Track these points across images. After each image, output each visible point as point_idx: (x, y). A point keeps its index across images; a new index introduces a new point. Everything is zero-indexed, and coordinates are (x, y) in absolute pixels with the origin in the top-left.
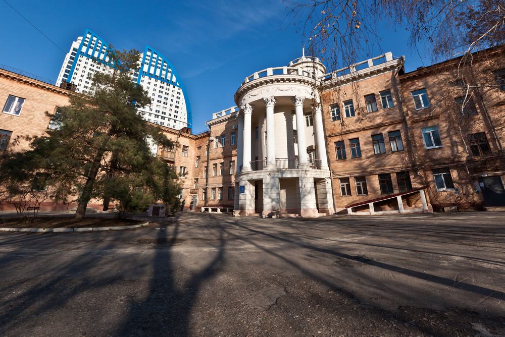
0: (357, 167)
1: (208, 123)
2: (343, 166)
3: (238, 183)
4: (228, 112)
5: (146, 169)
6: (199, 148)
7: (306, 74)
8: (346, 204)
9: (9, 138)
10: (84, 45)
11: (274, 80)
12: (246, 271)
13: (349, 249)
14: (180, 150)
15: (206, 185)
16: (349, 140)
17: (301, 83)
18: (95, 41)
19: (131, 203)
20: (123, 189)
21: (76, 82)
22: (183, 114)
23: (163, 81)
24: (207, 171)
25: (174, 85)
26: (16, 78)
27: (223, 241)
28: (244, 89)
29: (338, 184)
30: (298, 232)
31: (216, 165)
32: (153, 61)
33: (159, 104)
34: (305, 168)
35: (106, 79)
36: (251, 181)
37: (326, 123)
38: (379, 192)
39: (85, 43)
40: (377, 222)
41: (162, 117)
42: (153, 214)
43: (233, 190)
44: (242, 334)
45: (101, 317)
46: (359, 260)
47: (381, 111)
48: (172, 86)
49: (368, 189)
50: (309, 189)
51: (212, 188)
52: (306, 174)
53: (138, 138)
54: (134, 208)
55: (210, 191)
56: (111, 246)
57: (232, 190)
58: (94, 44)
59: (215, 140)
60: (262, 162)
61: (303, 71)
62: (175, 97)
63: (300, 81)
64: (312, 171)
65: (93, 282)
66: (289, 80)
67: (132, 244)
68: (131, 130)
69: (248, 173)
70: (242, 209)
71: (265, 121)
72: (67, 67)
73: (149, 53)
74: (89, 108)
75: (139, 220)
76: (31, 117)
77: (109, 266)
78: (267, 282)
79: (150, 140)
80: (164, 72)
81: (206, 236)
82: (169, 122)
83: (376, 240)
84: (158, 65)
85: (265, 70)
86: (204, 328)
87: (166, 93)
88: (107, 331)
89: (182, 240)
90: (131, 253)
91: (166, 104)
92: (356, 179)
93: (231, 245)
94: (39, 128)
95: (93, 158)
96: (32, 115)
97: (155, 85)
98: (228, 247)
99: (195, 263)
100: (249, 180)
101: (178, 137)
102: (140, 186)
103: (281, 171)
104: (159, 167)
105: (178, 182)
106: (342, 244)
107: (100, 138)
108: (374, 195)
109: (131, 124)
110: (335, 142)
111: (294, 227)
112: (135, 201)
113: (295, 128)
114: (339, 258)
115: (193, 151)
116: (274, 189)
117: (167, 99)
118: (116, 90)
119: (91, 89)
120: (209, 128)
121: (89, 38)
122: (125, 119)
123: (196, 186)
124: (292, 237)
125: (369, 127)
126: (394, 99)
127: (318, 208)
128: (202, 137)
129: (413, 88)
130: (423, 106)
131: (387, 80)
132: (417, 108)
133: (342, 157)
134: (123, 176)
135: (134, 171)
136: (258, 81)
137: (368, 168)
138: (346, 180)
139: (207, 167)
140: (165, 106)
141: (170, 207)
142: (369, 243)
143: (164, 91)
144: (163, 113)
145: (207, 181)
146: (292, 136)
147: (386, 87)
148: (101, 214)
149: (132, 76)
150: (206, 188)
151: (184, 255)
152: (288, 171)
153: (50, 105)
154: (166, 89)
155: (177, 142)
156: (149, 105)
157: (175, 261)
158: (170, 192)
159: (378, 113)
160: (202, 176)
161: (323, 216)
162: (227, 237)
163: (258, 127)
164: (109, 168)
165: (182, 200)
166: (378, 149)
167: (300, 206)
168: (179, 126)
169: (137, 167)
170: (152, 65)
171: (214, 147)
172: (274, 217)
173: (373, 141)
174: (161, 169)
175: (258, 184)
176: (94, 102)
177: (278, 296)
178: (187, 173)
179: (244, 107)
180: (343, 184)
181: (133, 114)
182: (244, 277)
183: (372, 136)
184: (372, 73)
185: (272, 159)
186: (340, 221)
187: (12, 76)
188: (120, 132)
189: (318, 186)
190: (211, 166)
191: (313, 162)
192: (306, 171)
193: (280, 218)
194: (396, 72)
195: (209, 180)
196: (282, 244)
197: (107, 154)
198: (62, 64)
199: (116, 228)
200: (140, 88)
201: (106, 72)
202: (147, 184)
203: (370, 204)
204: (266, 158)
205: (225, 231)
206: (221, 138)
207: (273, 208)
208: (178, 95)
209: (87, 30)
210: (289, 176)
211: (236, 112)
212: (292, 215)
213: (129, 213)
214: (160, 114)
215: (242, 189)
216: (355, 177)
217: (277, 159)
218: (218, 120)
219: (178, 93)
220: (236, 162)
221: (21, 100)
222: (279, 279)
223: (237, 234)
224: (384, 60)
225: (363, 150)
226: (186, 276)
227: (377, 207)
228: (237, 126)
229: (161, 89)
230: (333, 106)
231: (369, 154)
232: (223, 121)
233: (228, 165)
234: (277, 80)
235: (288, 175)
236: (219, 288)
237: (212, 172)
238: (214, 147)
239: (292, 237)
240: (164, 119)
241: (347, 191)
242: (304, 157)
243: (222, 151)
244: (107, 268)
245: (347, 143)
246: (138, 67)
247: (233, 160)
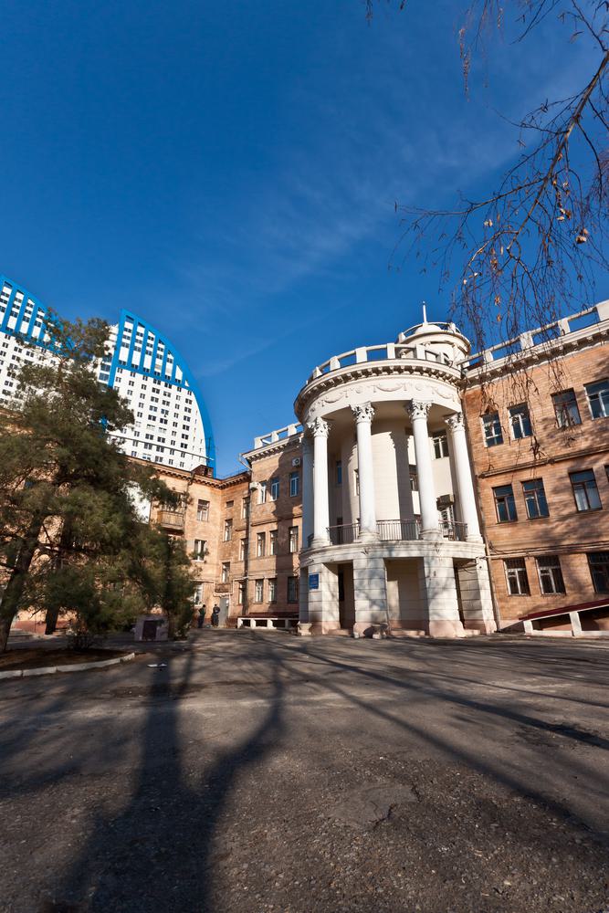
0: (540, 537)
1: (245, 456)
2: (512, 536)
3: (305, 570)
4: (282, 435)
5: (128, 546)
6: (230, 503)
8: (520, 613)
12: (327, 748)
13: (541, 710)
14: (193, 508)
15: (246, 575)
16: (522, 482)
17: (422, 374)
18: (20, 301)
19: (98, 617)
20: (83, 589)
22: (198, 440)
23: (158, 378)
24: (246, 547)
25: (180, 386)
27: (279, 686)
28: (312, 390)
29: (503, 571)
30: (427, 668)
31: (262, 535)
32: (137, 341)
33: (151, 422)
34: (434, 538)
35: (45, 376)
37: (474, 450)
38: (591, 589)
40: (592, 654)
41: (158, 447)
42: (144, 635)
43: (297, 583)
44: (321, 878)
45: (31, 853)
46: (567, 734)
47: (588, 425)
48: (176, 387)
49: (565, 582)
50: (444, 580)
51: (256, 580)
52: (438, 551)
53: (112, 489)
54: (105, 625)
55: (252, 586)
56: (59, 706)
57: (293, 582)
58: (18, 307)
59: (261, 489)
60: (351, 528)
61: (426, 351)
62: (182, 408)
63: (427, 367)
64: (448, 545)
65: (18, 783)
66: (399, 370)
67: (100, 699)
68: (97, 475)
69: (324, 550)
70: (315, 621)
71: (355, 451)
73: (129, 325)
74: (13, 432)
75: (116, 648)
77: (52, 746)
78: (368, 772)
79: (134, 492)
80: (159, 362)
81: (246, 675)
82: (171, 457)
83: (596, 693)
84: (148, 348)
85: (352, 352)
86: (245, 866)
87: (164, 402)
88: (41, 883)
89: (199, 687)
90: (96, 718)
93: (295, 694)
95: (24, 530)
97: (144, 387)
98: (289, 698)
99: (224, 733)
100: (325, 564)
101: (189, 485)
102: (118, 579)
103: (387, 545)
104: (153, 542)
105: (191, 570)
106: (524, 697)
107: (36, 491)
108: (578, 595)
109: (97, 463)
110: (493, 488)
111: (418, 659)
112: (106, 610)
113: (412, 461)
114: (522, 727)
115: (217, 511)
116: (376, 580)
117: (167, 412)
118: (65, 398)
119: (16, 396)
120: (247, 466)
121: (7, 296)
122: (85, 452)
123: (227, 578)
124: (416, 679)
125: (564, 456)
127: (462, 620)
128: (234, 484)
131: (599, 360)
133: (508, 516)
134: (82, 564)
135: (105, 554)
136: (338, 374)
137: (564, 540)
139: (246, 540)
140: (163, 425)
141: (176, 620)
142: (582, 697)
143: (161, 397)
144: (159, 439)
145: (246, 567)
146: (408, 477)
147: (596, 375)
148: (42, 641)
149: (98, 371)
151: (202, 716)
152: (402, 544)
154: (165, 395)
155: (186, 494)
156: (130, 425)
157: (184, 728)
158: (176, 590)
159: (583, 428)
160: (236, 559)
161: (474, 636)
162: (288, 678)
163: (340, 462)
164: (57, 549)
165: (199, 606)
166: (585, 500)
167: (428, 615)
168: (191, 464)
169: (111, 544)
170: (135, 348)
171: (259, 502)
172: (376, 636)
173: (573, 484)
174: (156, 546)
175: (344, 571)
176: (22, 421)
177: (392, 801)
178: (207, 553)
179: (314, 424)
181: (100, 443)
182: (323, 759)
183: (571, 474)
185: (370, 522)
186: (507, 646)
188: (76, 479)
189: (462, 575)
190: (254, 538)
191: (450, 528)
192: (436, 544)
193: (388, 638)
195: (251, 564)
196: (398, 691)
197: (50, 522)
199: (70, 668)
200: (113, 394)
201: (47, 363)
202: (130, 575)
203: (571, 614)
204: (359, 520)
205: (283, 665)
206: (271, 484)
207: (374, 619)
208: (188, 405)
210: (403, 554)
211: (298, 434)
212: (412, 634)
213: (96, 636)
214: (155, 441)
215: (314, 581)
216: (536, 557)
217: (380, 522)
218: (266, 449)
219: (187, 401)
220: (300, 528)
222: (392, 765)
223: (307, 671)
225: (553, 504)
226: (206, 759)
227: (588, 621)
229: (155, 395)
231: (565, 512)
232: (275, 451)
233: (287, 535)
234: (377, 371)
236: (273, 784)
237: (255, 550)
238: (259, 502)
239: (416, 679)
241: (521, 585)
242: (433, 518)
243: (274, 508)
244: (49, 750)
245: (518, 489)
246: (106, 353)
247: (294, 525)
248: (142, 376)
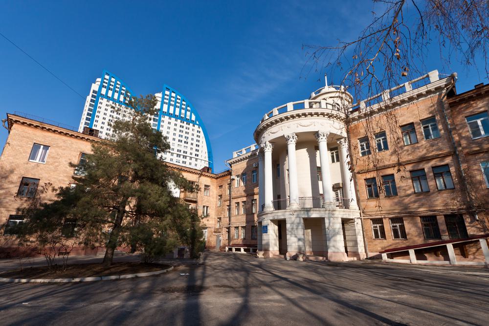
1: (228, 162)
3: (260, 223)
4: (248, 150)
6: (221, 186)
7: (330, 107)
9: (37, 185)
10: (103, 86)
11: (301, 114)
15: (229, 224)
17: (324, 116)
21: (98, 128)
22: (204, 152)
23: (183, 120)
24: (229, 210)
25: (194, 124)
26: (39, 126)
29: (370, 225)
32: (172, 101)
33: (180, 143)
36: (273, 221)
39: (104, 84)
42: (178, 255)
43: (256, 229)
51: (235, 227)
55: (233, 231)
60: (285, 201)
61: (327, 103)
62: (195, 135)
63: (323, 115)
66: (311, 114)
72: (87, 115)
73: (167, 93)
76: (57, 164)
79: (171, 184)
80: (183, 111)
84: (177, 104)
85: (285, 105)
87: (186, 133)
91: (187, 143)
92: (391, 220)
94: (65, 175)
96: (57, 162)
101: (199, 177)
113: (318, 165)
115: (214, 191)
123: (220, 226)
126: (440, 127)
127: (347, 252)
128: (223, 176)
129: (468, 112)
130: (483, 133)
132: (474, 137)
133: (373, 194)
136: (277, 118)
138: (379, 221)
139: (229, 206)
140: (186, 145)
143: (184, 130)
144: (184, 152)
145: (230, 220)
146: (316, 173)
150: (229, 227)
153: (74, 151)
154: (186, 129)
160: (224, 216)
166: (419, 186)
168: (202, 164)
170: (171, 105)
175: (281, 224)
179: (264, 145)
180: (376, 225)
184: (411, 99)
187: (35, 124)
190: (233, 205)
191: (340, 201)
194: (443, 95)
195: (232, 219)
198: (83, 112)
204: (289, 196)
207: (300, 249)
208: (198, 134)
209: (104, 71)
211: (256, 150)
215: (265, 229)
216: (390, 218)
218: (239, 158)
220: (258, 200)
221: (46, 147)
224: (427, 81)
227: (420, 255)
228: (258, 164)
229: (181, 129)
230: (362, 140)
232: (244, 159)
233: (250, 204)
234: (299, 116)
235: (314, 215)
237: (234, 211)
238: (236, 186)
240: (186, 158)
241: (380, 234)
242: (331, 196)
243: (244, 189)
245: (379, 181)
248: (175, 119)
